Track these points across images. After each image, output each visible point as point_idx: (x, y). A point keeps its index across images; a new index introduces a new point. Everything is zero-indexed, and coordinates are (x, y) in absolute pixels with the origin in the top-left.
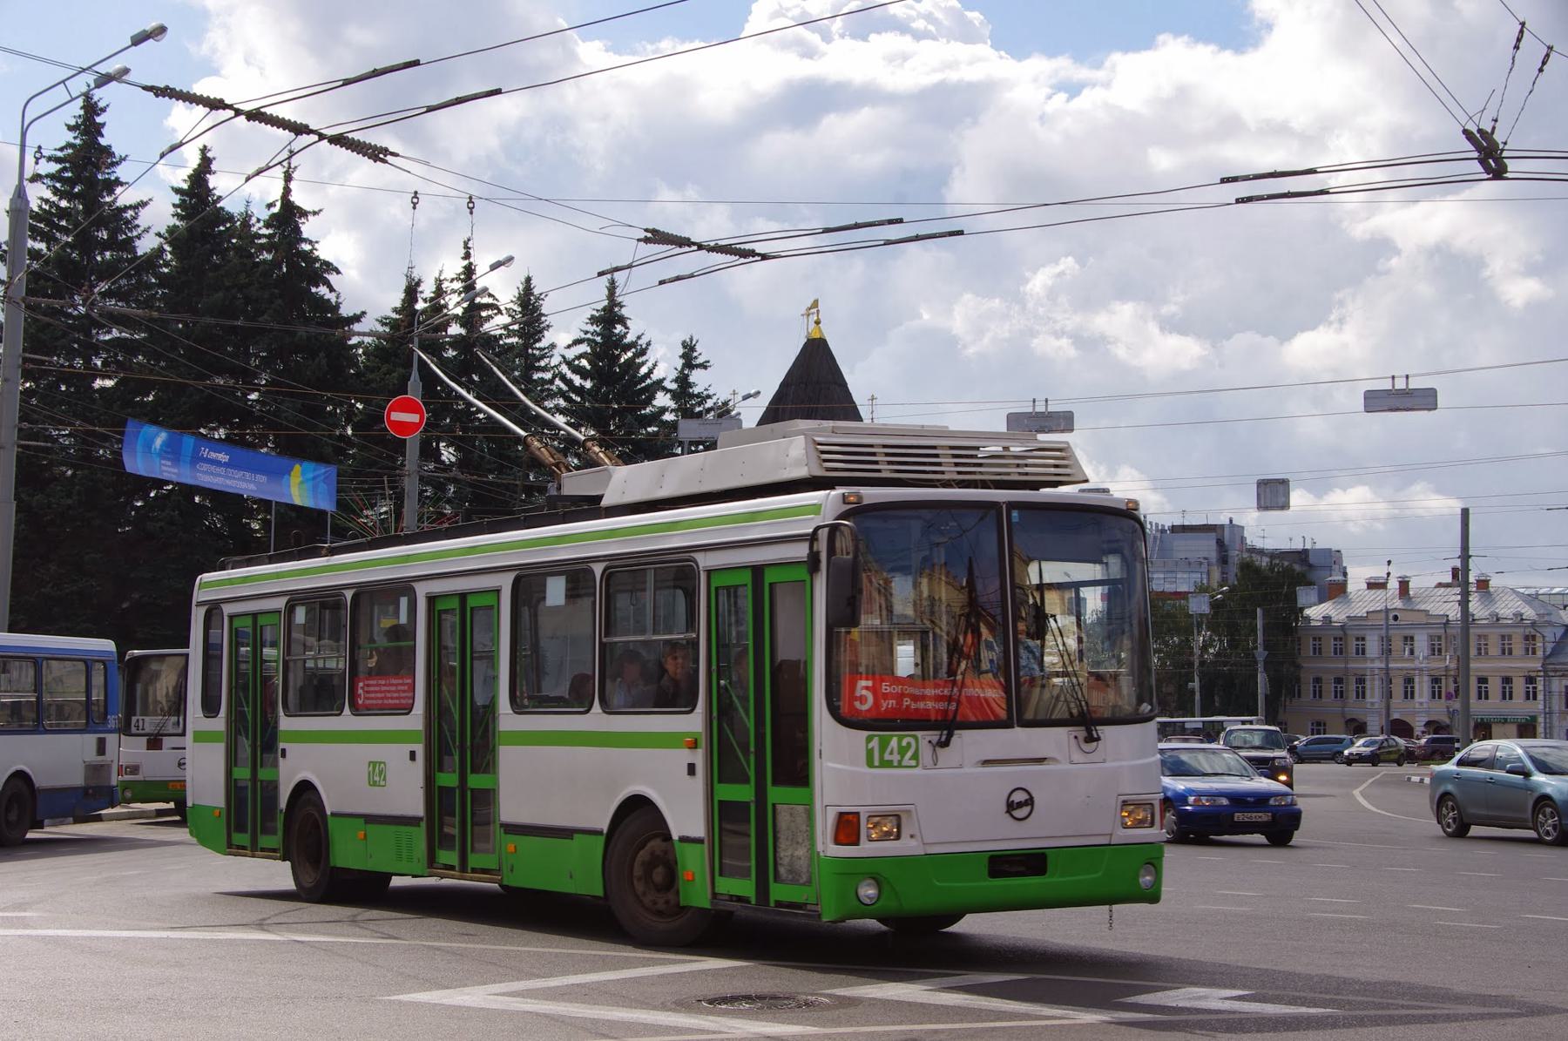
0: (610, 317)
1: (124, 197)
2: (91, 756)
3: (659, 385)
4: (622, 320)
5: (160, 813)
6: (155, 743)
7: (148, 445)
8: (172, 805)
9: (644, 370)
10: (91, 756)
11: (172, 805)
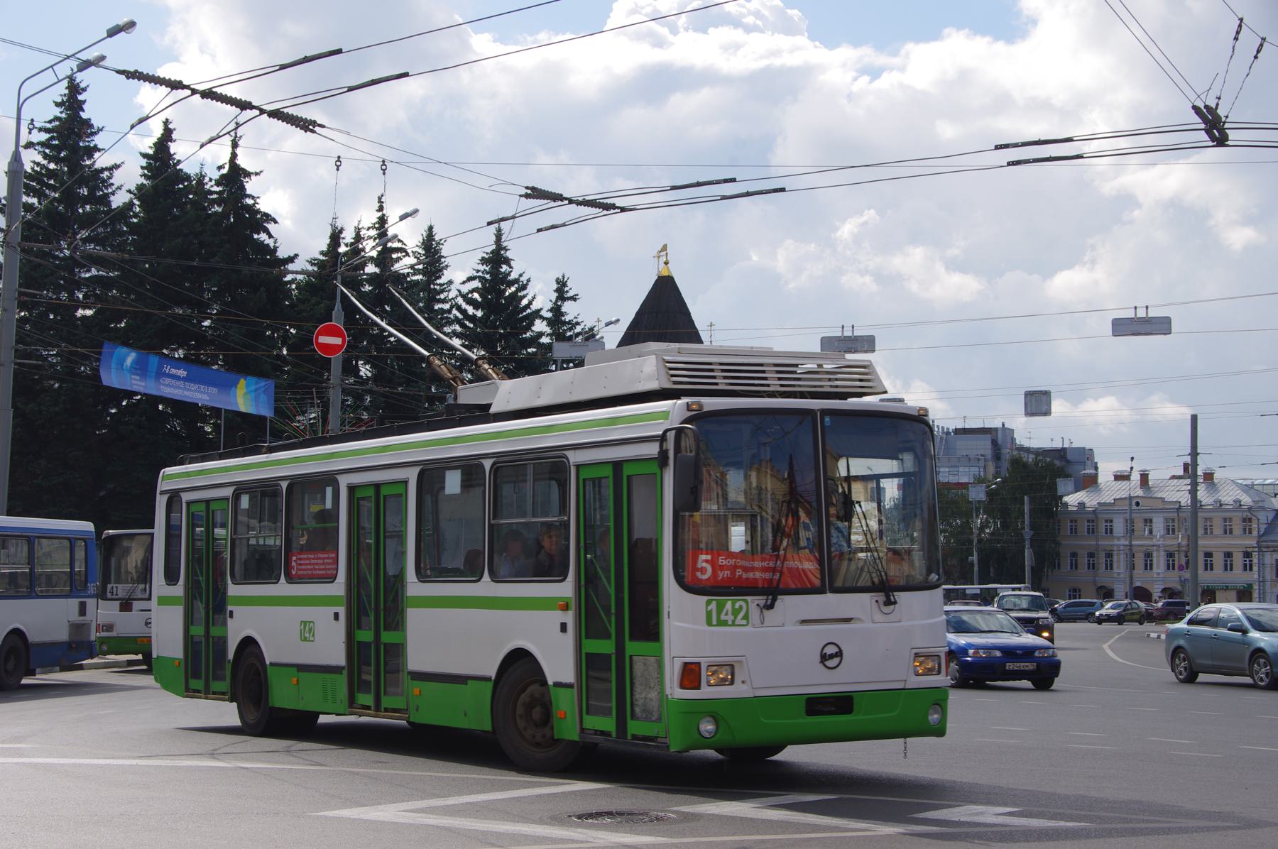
0: (497, 259)
1: (101, 161)
2: (75, 617)
3: (537, 314)
4: (507, 261)
5: (130, 663)
6: (126, 606)
7: (121, 363)
8: (140, 657)
9: (525, 302)
10: (75, 617)
11: (140, 657)
